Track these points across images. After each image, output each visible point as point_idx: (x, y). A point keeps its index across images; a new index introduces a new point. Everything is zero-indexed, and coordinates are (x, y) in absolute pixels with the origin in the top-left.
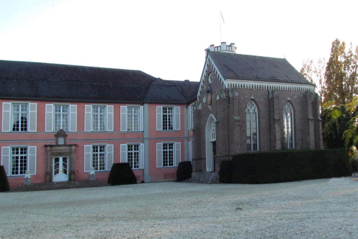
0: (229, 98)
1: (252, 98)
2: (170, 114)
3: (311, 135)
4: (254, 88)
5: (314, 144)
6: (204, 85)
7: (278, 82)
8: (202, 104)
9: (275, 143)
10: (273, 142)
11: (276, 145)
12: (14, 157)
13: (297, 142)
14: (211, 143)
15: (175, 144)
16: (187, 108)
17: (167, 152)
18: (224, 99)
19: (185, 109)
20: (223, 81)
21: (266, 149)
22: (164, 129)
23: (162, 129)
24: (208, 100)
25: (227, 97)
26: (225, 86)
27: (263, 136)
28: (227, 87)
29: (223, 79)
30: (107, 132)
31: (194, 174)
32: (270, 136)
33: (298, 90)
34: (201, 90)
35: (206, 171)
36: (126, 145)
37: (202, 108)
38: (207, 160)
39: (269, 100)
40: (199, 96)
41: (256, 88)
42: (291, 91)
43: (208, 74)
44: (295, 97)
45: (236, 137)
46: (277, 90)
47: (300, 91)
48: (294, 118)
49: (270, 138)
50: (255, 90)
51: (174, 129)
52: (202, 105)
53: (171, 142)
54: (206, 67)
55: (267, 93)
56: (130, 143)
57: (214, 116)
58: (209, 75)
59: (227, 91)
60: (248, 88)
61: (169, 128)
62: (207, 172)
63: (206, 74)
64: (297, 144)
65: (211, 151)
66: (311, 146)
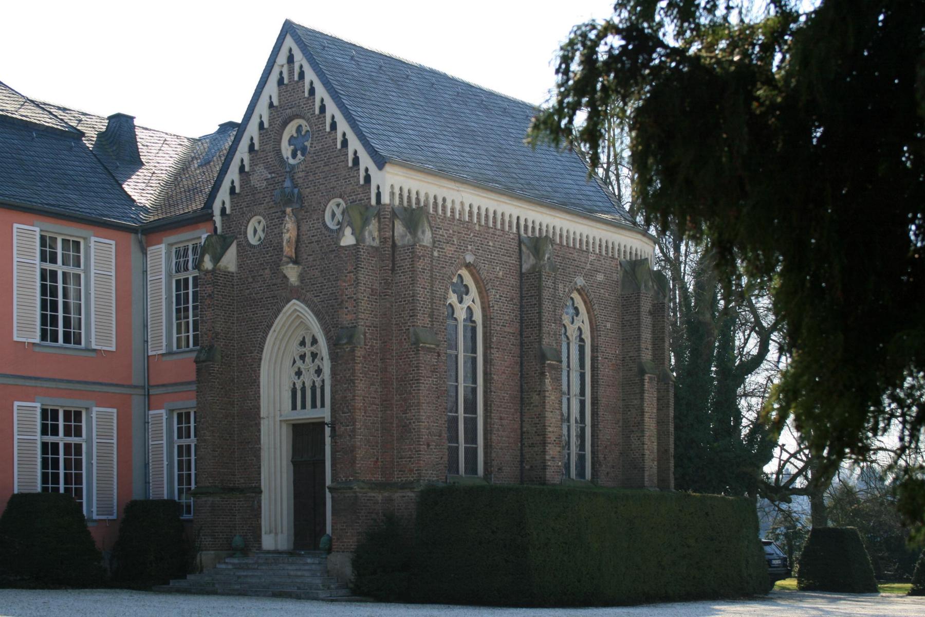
0: (394, 245)
1: (470, 258)
2: (71, 270)
3: (647, 434)
4: (475, 220)
5: (655, 470)
6: (253, 162)
7: (483, 189)
8: (238, 245)
9: (544, 452)
10: (532, 446)
11: (544, 461)
12: (52, 435)
13: (601, 456)
14: (284, 426)
15: (94, 415)
16: (144, 253)
17: (55, 446)
18: (372, 247)
19: (136, 254)
20: (367, 170)
21: (506, 477)
22: (44, 337)
23: (37, 340)
24: (286, 236)
25: (383, 240)
26: (379, 195)
27: (501, 419)
28: (386, 199)
29: (366, 161)
30: (95, 350)
31: (206, 557)
32: (522, 421)
33: (610, 255)
34: (237, 184)
35: (260, 547)
36: (38, 405)
37: (240, 266)
38: (264, 497)
39: (521, 275)
40: (223, 210)
41: (483, 223)
42: (587, 251)
43: (279, 121)
44: (600, 277)
45: (427, 419)
46: (552, 242)
47: (613, 258)
48: (594, 359)
49: (519, 431)
50: (477, 227)
51: (88, 341)
52: (238, 251)
53: (73, 404)
54: (272, 88)
55: (514, 244)
56: (52, 403)
57: (312, 311)
58: (285, 124)
59: (386, 215)
60: (457, 216)
61: (67, 339)
62: (269, 552)
63: (272, 120)
64: (600, 465)
65: (285, 463)
66: (549, 473)
